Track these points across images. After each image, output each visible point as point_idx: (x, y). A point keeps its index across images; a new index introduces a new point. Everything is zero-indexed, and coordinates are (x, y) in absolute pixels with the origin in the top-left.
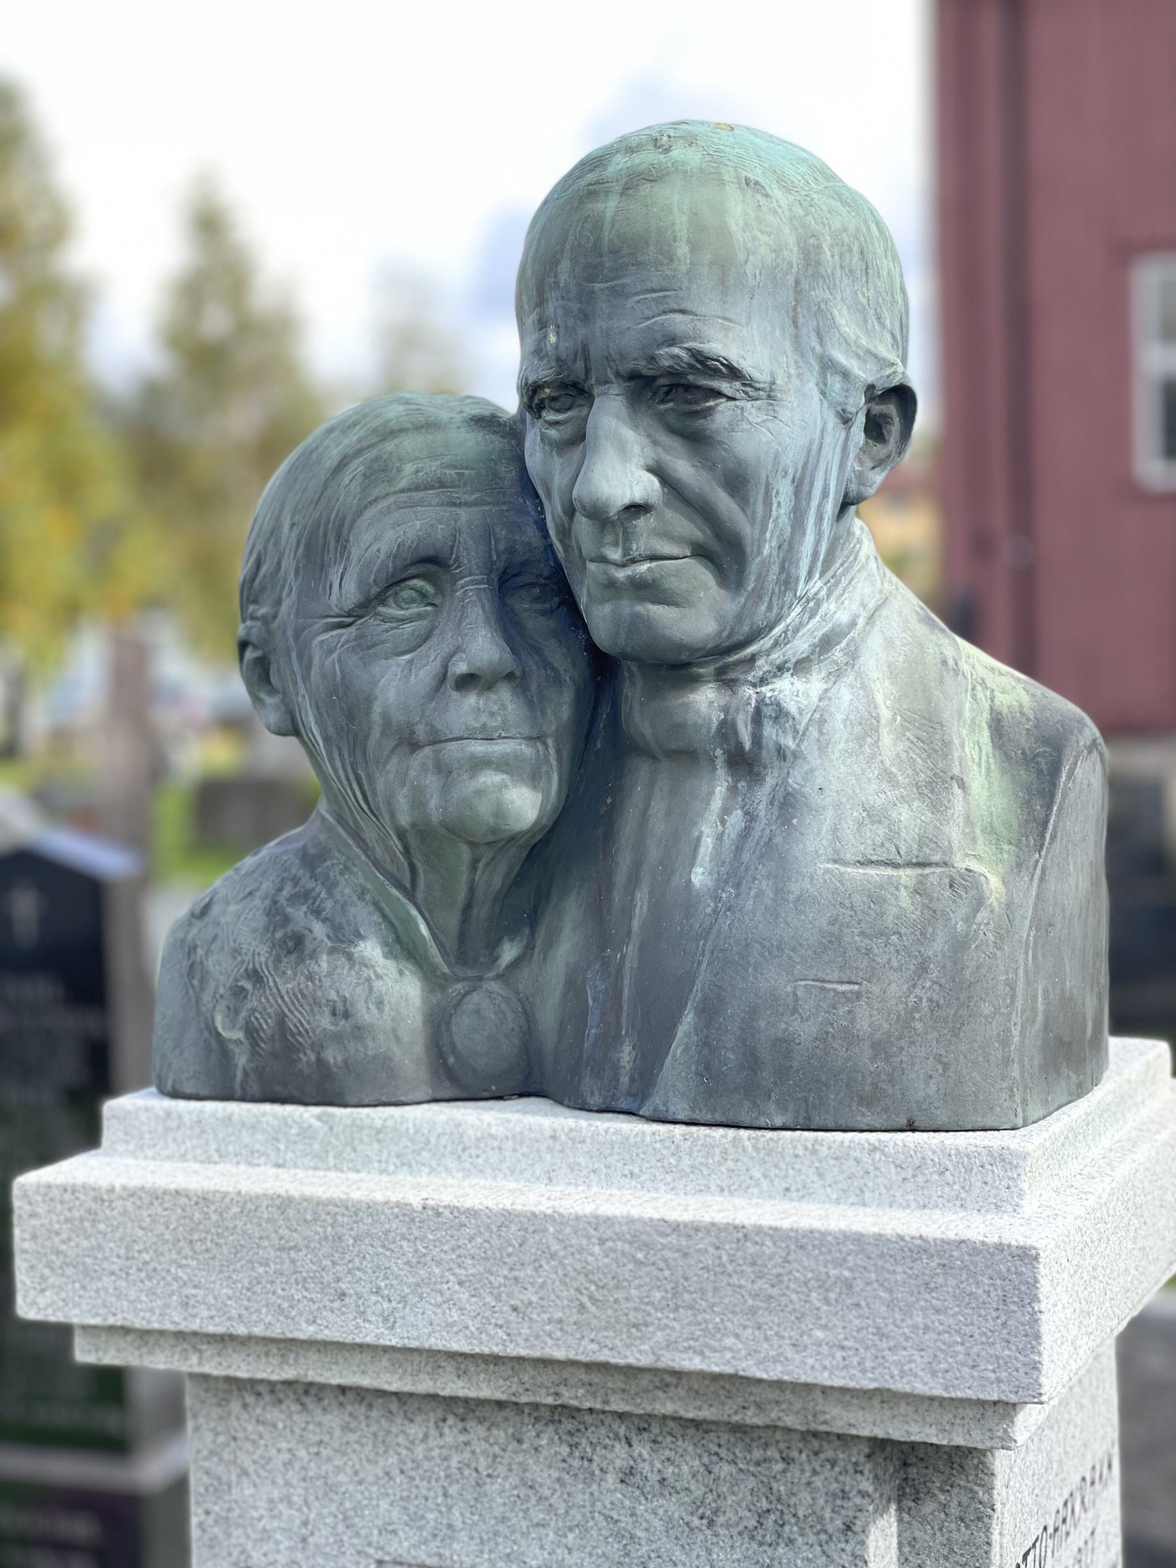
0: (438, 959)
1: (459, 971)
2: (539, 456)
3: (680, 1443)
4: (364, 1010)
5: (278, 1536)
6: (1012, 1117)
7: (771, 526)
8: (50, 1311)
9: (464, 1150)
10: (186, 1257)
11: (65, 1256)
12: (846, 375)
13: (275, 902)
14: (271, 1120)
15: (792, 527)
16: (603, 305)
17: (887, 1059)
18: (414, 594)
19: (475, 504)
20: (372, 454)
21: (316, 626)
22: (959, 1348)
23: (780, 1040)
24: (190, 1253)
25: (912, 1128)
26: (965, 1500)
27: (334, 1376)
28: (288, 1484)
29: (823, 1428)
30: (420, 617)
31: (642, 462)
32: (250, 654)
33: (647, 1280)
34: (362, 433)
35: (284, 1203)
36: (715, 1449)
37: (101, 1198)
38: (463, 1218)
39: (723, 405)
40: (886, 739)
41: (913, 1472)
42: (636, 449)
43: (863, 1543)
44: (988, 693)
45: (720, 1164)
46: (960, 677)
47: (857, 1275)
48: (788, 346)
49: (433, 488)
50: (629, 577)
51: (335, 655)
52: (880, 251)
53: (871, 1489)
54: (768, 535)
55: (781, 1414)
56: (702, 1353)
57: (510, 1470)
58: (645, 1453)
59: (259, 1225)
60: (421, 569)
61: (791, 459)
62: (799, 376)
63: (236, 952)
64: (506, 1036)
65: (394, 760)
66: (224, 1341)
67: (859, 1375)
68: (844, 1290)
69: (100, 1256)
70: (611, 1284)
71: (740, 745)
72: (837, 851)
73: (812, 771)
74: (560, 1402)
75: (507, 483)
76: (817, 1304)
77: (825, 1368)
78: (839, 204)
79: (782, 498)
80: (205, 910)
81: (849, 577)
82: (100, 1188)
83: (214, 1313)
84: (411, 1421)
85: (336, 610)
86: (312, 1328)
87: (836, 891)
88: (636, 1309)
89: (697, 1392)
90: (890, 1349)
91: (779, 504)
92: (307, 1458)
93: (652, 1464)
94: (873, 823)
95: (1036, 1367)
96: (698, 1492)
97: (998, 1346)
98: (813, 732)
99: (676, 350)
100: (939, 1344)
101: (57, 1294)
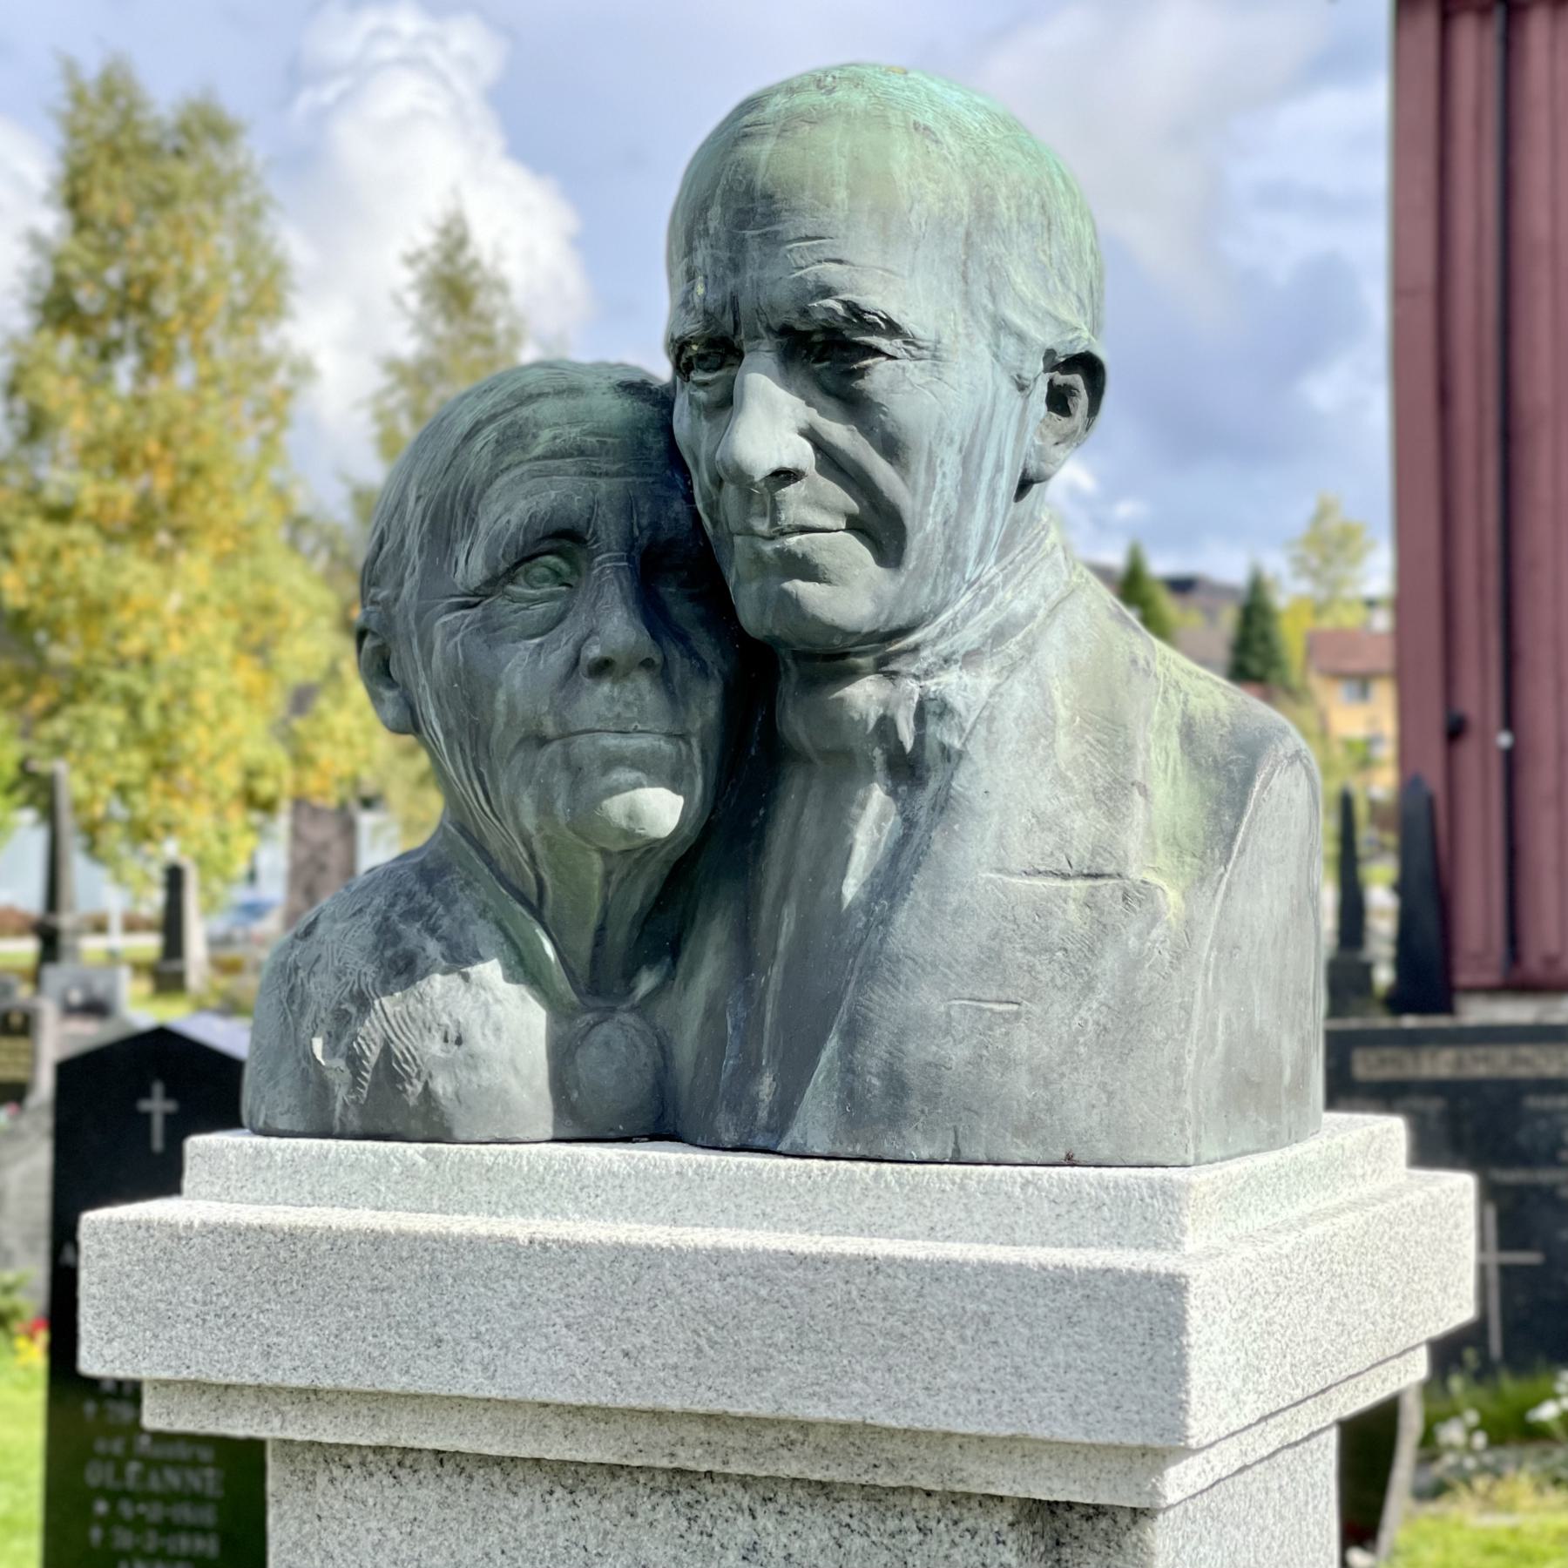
1: (590, 1002)
2: (686, 421)
3: (808, 1514)
4: (479, 1036)
6: (1182, 1153)
7: (935, 499)
8: (117, 1363)
9: (581, 1189)
10: (269, 1301)
11: (137, 1301)
12: (1021, 337)
13: (386, 919)
14: (372, 1159)
15: (960, 501)
16: (754, 253)
17: (1047, 1084)
18: (547, 572)
19: (617, 474)
21: (439, 607)
22: (1103, 1388)
23: (930, 1064)
24: (274, 1296)
25: (1070, 1162)
27: (429, 1439)
29: (959, 1488)
30: (552, 597)
31: (793, 424)
32: (368, 643)
33: (771, 1319)
34: (498, 398)
35: (378, 1239)
36: (847, 1520)
37: (178, 1235)
39: (879, 366)
40: (1063, 740)
41: (1066, 1552)
42: (787, 410)
44: (1181, 696)
46: (1152, 678)
47: (995, 1309)
48: (956, 302)
49: (571, 456)
50: (776, 551)
51: (458, 638)
52: (1066, 207)
54: (931, 509)
55: (915, 1472)
57: (622, 1548)
58: (770, 1526)
59: (350, 1264)
60: (555, 544)
61: (958, 426)
62: (968, 336)
64: (639, 1072)
65: (521, 755)
66: (309, 1395)
67: (995, 1420)
68: (982, 1327)
69: (174, 1301)
70: (731, 1324)
72: (1000, 859)
73: (978, 772)
74: (675, 1465)
75: (654, 453)
76: (952, 1343)
77: (959, 1413)
78: (1020, 156)
79: (947, 469)
80: (309, 931)
81: (1030, 565)
82: (177, 1224)
83: (298, 1363)
84: (515, 1494)
85: (462, 589)
86: (404, 1379)
87: (999, 903)
88: (756, 1352)
89: (824, 1449)
90: (1028, 1391)
91: (944, 475)
92: (398, 1540)
93: (777, 1538)
94: (1043, 830)
95: (1182, 1406)
97: (1143, 1385)
98: (982, 730)
99: (830, 303)
100: (1081, 1384)
101: (126, 1344)
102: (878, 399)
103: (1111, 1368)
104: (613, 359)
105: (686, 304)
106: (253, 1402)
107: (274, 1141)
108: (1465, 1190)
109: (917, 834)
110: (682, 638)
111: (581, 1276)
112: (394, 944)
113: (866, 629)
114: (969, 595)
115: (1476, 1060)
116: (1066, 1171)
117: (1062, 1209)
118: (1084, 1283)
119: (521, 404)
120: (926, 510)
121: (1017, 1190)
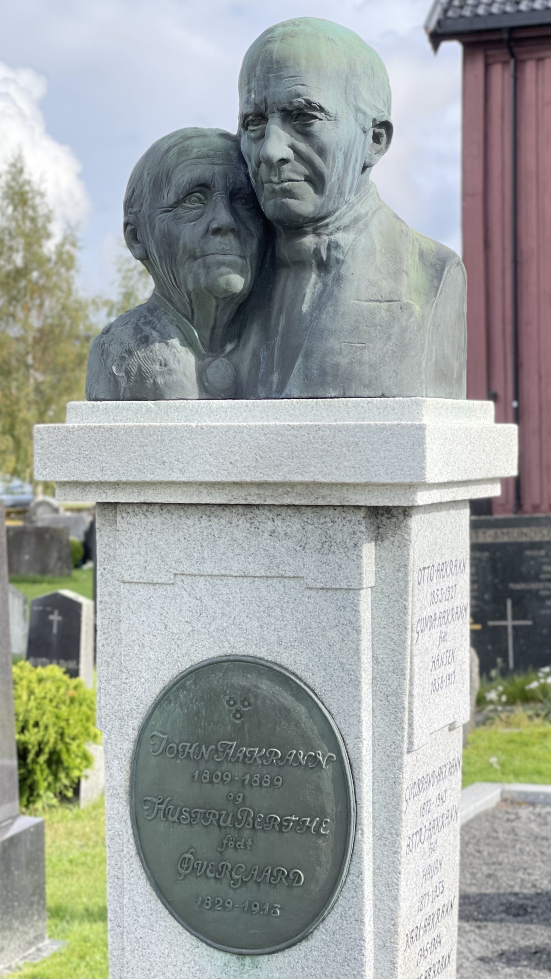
0: (201, 347)
1: (210, 354)
2: (246, 145)
5: (135, 567)
7: (335, 170)
12: (365, 114)
14: (135, 406)
16: (272, 82)
17: (375, 370)
19: (221, 164)
20: (181, 145)
22: (397, 464)
25: (383, 396)
26: (400, 539)
28: (139, 547)
30: (198, 208)
32: (129, 228)
36: (306, 520)
38: (212, 429)
40: (378, 257)
41: (381, 530)
43: (361, 550)
45: (310, 412)
49: (204, 158)
51: (165, 222)
53: (364, 530)
56: (302, 474)
63: (121, 343)
65: (187, 263)
70: (268, 450)
71: (322, 258)
79: (339, 159)
85: (166, 205)
86: (152, 476)
93: (282, 528)
95: (424, 468)
96: (299, 537)
98: (350, 253)
99: (300, 99)
102: (316, 134)
103: (400, 457)
104: (214, 127)
105: (248, 102)
106: (95, 490)
107: (99, 402)
108: (514, 429)
109: (328, 289)
110: (244, 223)
111: (215, 437)
112: (141, 333)
113: (311, 216)
114: (345, 206)
115: (503, 534)
116: (383, 399)
117: (381, 411)
118: (391, 429)
119: (185, 140)
120: (332, 176)
121: (365, 405)
